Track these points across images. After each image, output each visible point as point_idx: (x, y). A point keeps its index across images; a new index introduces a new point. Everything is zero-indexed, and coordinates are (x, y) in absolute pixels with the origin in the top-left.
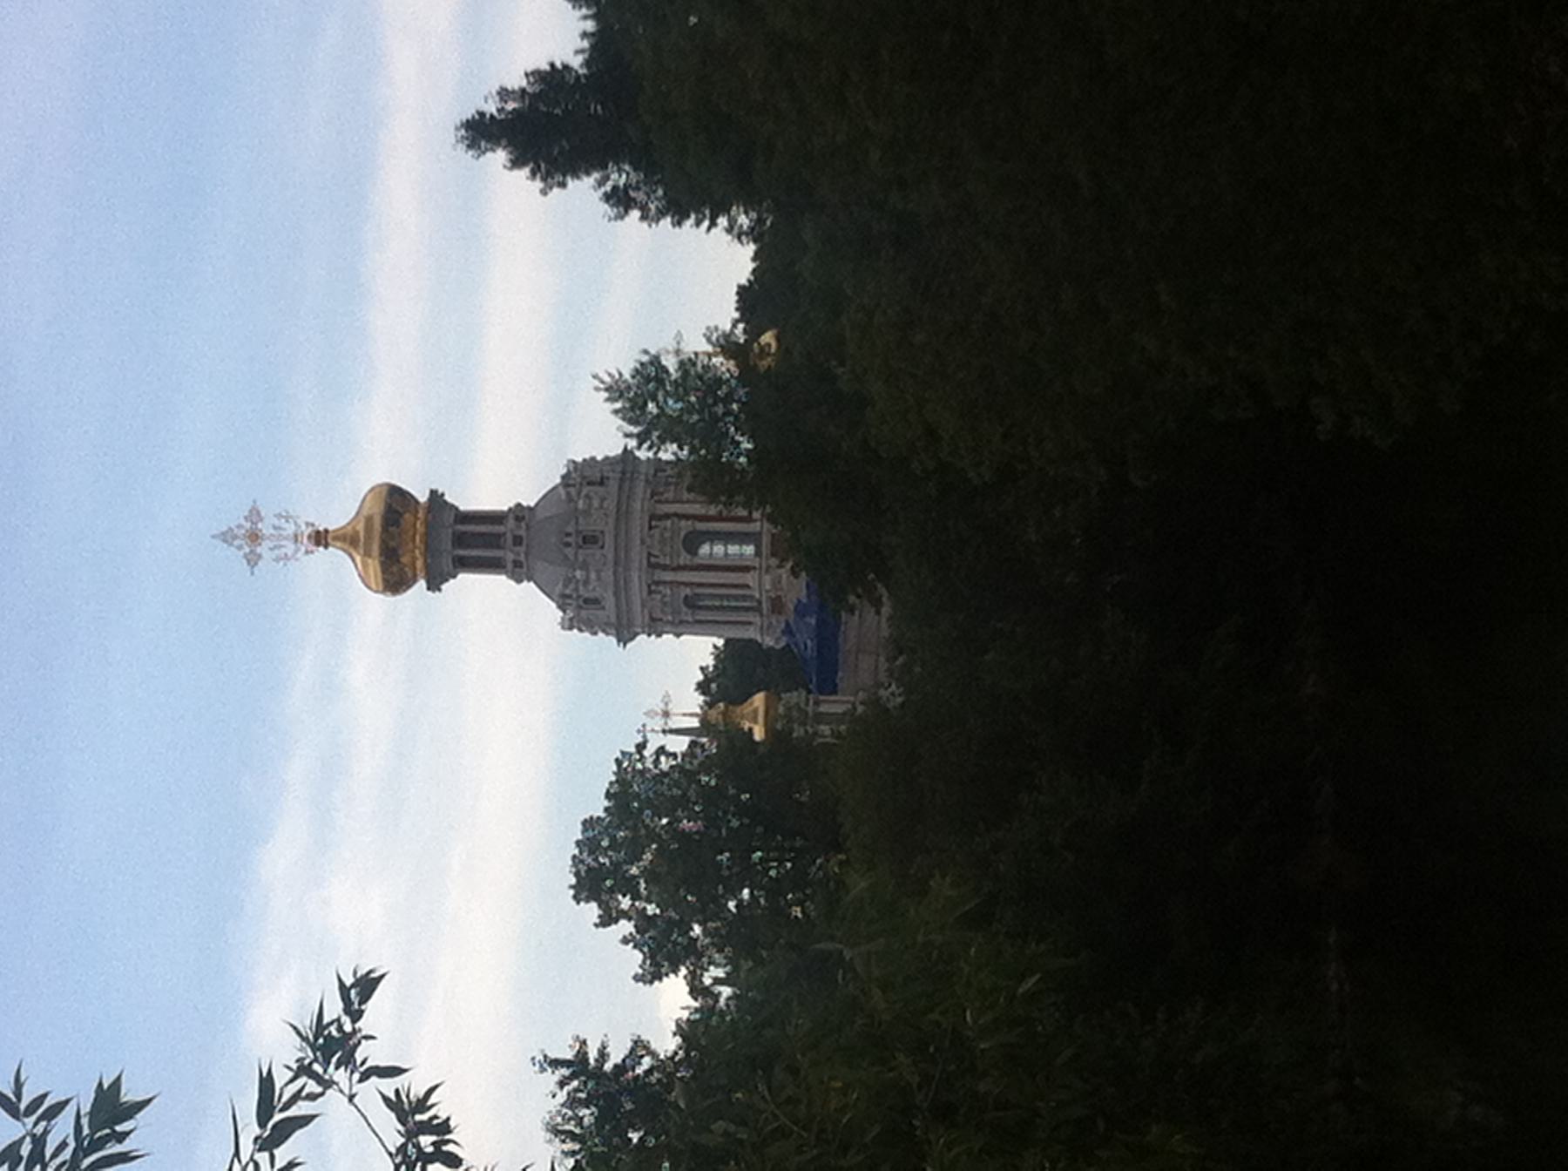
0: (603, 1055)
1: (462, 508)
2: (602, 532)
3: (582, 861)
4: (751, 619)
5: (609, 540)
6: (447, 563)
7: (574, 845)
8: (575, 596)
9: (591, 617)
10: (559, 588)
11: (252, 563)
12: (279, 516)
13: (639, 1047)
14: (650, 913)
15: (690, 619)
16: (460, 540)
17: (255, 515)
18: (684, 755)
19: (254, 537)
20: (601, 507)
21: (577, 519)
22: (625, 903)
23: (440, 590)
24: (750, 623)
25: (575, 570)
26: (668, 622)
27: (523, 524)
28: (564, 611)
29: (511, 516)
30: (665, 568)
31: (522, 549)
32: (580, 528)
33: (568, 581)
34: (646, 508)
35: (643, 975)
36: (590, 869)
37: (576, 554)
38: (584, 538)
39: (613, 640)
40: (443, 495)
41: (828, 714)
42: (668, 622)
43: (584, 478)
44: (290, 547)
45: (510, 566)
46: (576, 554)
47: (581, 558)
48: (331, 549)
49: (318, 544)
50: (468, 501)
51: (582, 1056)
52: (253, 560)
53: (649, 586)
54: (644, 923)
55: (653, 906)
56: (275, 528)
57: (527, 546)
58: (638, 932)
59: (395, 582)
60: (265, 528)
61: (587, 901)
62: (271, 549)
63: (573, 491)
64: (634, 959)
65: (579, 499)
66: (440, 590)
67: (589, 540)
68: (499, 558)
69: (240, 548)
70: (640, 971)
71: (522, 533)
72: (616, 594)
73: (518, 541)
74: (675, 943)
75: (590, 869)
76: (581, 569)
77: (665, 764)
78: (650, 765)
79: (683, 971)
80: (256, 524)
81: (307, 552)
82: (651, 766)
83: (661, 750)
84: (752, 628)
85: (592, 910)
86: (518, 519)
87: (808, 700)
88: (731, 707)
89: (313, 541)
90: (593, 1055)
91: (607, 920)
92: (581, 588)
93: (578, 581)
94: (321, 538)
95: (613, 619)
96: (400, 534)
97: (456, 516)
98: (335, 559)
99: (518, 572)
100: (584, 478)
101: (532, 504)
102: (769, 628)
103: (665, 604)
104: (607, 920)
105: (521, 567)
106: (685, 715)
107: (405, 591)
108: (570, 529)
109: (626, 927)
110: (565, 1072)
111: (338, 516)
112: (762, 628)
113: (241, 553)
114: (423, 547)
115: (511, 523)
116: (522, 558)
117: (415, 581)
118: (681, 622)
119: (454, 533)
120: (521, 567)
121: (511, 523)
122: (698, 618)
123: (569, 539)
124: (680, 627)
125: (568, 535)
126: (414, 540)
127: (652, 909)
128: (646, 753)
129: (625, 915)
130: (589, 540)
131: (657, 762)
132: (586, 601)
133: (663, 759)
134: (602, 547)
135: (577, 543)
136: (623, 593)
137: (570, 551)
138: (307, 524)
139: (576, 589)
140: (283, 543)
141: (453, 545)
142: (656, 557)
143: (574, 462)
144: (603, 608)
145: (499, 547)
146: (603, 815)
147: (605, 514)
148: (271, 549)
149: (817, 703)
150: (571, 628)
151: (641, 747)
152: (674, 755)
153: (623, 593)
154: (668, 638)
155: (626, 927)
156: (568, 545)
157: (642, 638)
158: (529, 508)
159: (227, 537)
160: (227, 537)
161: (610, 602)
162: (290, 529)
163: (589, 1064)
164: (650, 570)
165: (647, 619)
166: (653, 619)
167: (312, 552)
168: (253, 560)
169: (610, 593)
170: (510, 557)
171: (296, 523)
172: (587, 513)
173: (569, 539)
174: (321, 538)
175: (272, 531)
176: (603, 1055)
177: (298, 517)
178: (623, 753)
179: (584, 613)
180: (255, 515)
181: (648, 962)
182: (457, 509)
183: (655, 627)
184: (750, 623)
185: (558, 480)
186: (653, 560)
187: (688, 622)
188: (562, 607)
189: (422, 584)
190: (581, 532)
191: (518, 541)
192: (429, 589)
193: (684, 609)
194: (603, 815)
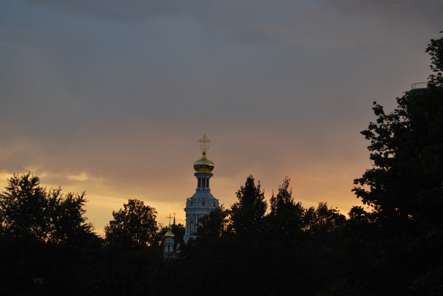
0: (83, 205)
1: (210, 180)
2: (205, 206)
3: (136, 201)
4: (188, 234)
6: (199, 177)
7: (139, 200)
8: (193, 200)
9: (189, 204)
10: (194, 198)
11: (200, 141)
12: (208, 146)
13: (84, 211)
14: (126, 214)
15: (189, 222)
16: (204, 179)
17: (209, 141)
18: (154, 220)
19: (204, 142)
20: (196, 205)
21: (207, 201)
22: (128, 209)
23: (195, 175)
24: (188, 233)
25: (198, 200)
26: (188, 218)
27: (206, 191)
28: (190, 199)
29: (208, 189)
31: (202, 191)
32: (206, 202)
33: (196, 199)
34: (196, 213)
35: (114, 212)
36: (134, 203)
37: (201, 201)
38: (204, 202)
39: (185, 208)
40: (212, 176)
41: (170, 248)
42: (188, 218)
43: (215, 202)
44: (202, 148)
45: (199, 188)
46: (201, 201)
47: (200, 202)
48: (202, 155)
49: (203, 153)
50: (212, 181)
51: (83, 201)
52: (200, 141)
53: (195, 214)
54: (124, 213)
55: (127, 215)
56: (206, 146)
57: (203, 192)
58: (122, 211)
59: (196, 167)
60: (206, 143)
61: (129, 202)
62: (202, 144)
63: (213, 200)
64: (117, 211)
65: (211, 201)
66: (195, 175)
67: (203, 203)
68: (200, 187)
69: (203, 139)
70: (115, 212)
71: (205, 191)
72: (193, 208)
73: (203, 190)
74: (120, 219)
75: (134, 203)
76: (198, 202)
77: (153, 217)
78: (153, 214)
79: (115, 220)
80: (207, 142)
81: (202, 151)
82: (153, 215)
83: (155, 216)
84: (187, 234)
85: (127, 203)
86: (208, 190)
87: (172, 244)
88: (171, 230)
89: (204, 152)
90: (82, 203)
91: (125, 206)
92: (195, 202)
93: (196, 201)
94: (204, 154)
95: (189, 208)
96: (205, 168)
97: (208, 178)
98: (201, 156)
99: (198, 190)
100: (215, 202)
101: (210, 193)
102: (187, 237)
103: (191, 217)
104: (125, 206)
105: (199, 191)
106: (170, 221)
107: (194, 169)
108: (206, 200)
109: (123, 209)
110: (80, 197)
111: (208, 157)
112: (187, 236)
113: (202, 139)
114: (203, 172)
115: (207, 189)
116: (200, 191)
117: (196, 171)
118: (188, 220)
119: (205, 178)
120: (199, 191)
121: (207, 189)
122: (189, 224)
123: (203, 199)
124: (187, 220)
125: (204, 199)
126: (204, 171)
127: (127, 214)
128: (155, 213)
129: (126, 209)
130: (203, 203)
131: (154, 215)
132: (192, 203)
133: (154, 217)
134: (202, 206)
135: (203, 201)
136: (193, 210)
137: (201, 199)
138: (207, 151)
139: (194, 201)
140: (203, 147)
141: (203, 178)
142: (200, 215)
143: (218, 201)
144: (191, 206)
145: (202, 186)
146: (144, 205)
147: (208, 206)
148: (202, 144)
149: (172, 246)
150: (187, 200)
151: (156, 212)
152: (155, 219)
153: (193, 210)
154: (185, 218)
155: (123, 209)
156: (202, 199)
157: (185, 213)
158: (210, 192)
159: (205, 136)
160: (205, 136)
161: (192, 207)
162: (206, 148)
163: (264, 214)
164: (198, 214)
165: (199, 214)
166: (189, 215)
167: (202, 152)
168: (200, 141)
169: (193, 207)
170: (201, 189)
171: (207, 149)
172: (209, 203)
173: (203, 199)
174: (204, 154)
175: (206, 145)
176: (83, 205)
177: (208, 149)
178: (155, 209)
179: (190, 202)
180: (209, 141)
181: (117, 213)
182: (210, 179)
183: (187, 215)
184: (188, 233)
185: (215, 198)
186: (200, 215)
187: (188, 222)
188: (191, 198)
189: (196, 172)
190: (205, 202)
191: (203, 190)
192: (195, 173)
193: (190, 221)
194: (144, 205)
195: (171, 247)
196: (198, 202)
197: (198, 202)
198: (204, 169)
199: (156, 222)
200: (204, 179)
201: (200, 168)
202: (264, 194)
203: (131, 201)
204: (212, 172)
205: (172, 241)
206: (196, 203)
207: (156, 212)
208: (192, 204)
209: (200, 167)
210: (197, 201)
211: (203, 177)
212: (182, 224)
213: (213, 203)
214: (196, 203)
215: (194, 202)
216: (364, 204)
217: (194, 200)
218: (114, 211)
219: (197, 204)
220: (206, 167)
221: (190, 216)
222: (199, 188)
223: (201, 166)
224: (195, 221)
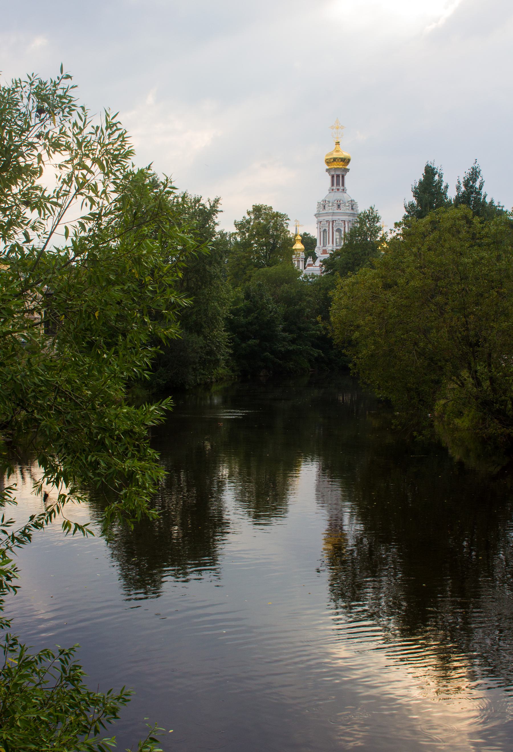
5: (338, 211)
16: (338, 176)
30: (333, 224)
33: (329, 202)
45: (332, 188)
54: (248, 222)
61: (253, 208)
64: (239, 219)
67: (339, 206)
68: (339, 185)
71: (340, 191)
77: (285, 225)
95: (320, 213)
108: (341, 202)
115: (342, 188)
117: (328, 166)
130: (339, 206)
137: (336, 202)
145: (337, 185)
155: (248, 217)
161: (325, 212)
168: (332, 127)
174: (338, 143)
179: (322, 206)
191: (338, 190)
195: (301, 262)
196: (333, 205)
197: (333, 205)
198: (338, 163)
199: (289, 231)
200: (338, 176)
201: (333, 162)
202: (448, 190)
203: (256, 206)
204: (347, 167)
205: (302, 255)
206: (329, 206)
207: (289, 219)
208: (324, 208)
209: (332, 160)
210: (331, 204)
211: (338, 173)
212: (307, 233)
213: (351, 205)
214: (329, 206)
215: (326, 206)
216: (253, 206)
217: (327, 202)
218: (235, 222)
219: (330, 208)
220: (340, 160)
221: (322, 223)
222: (332, 188)
223: (335, 159)
224: (345, 229)
